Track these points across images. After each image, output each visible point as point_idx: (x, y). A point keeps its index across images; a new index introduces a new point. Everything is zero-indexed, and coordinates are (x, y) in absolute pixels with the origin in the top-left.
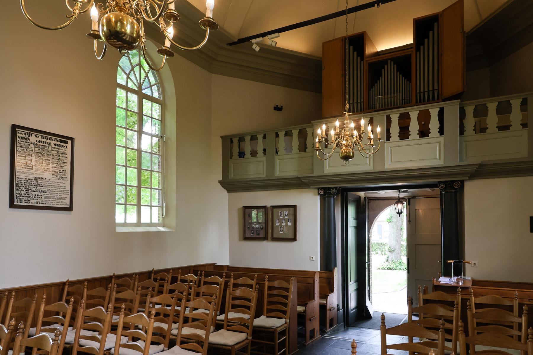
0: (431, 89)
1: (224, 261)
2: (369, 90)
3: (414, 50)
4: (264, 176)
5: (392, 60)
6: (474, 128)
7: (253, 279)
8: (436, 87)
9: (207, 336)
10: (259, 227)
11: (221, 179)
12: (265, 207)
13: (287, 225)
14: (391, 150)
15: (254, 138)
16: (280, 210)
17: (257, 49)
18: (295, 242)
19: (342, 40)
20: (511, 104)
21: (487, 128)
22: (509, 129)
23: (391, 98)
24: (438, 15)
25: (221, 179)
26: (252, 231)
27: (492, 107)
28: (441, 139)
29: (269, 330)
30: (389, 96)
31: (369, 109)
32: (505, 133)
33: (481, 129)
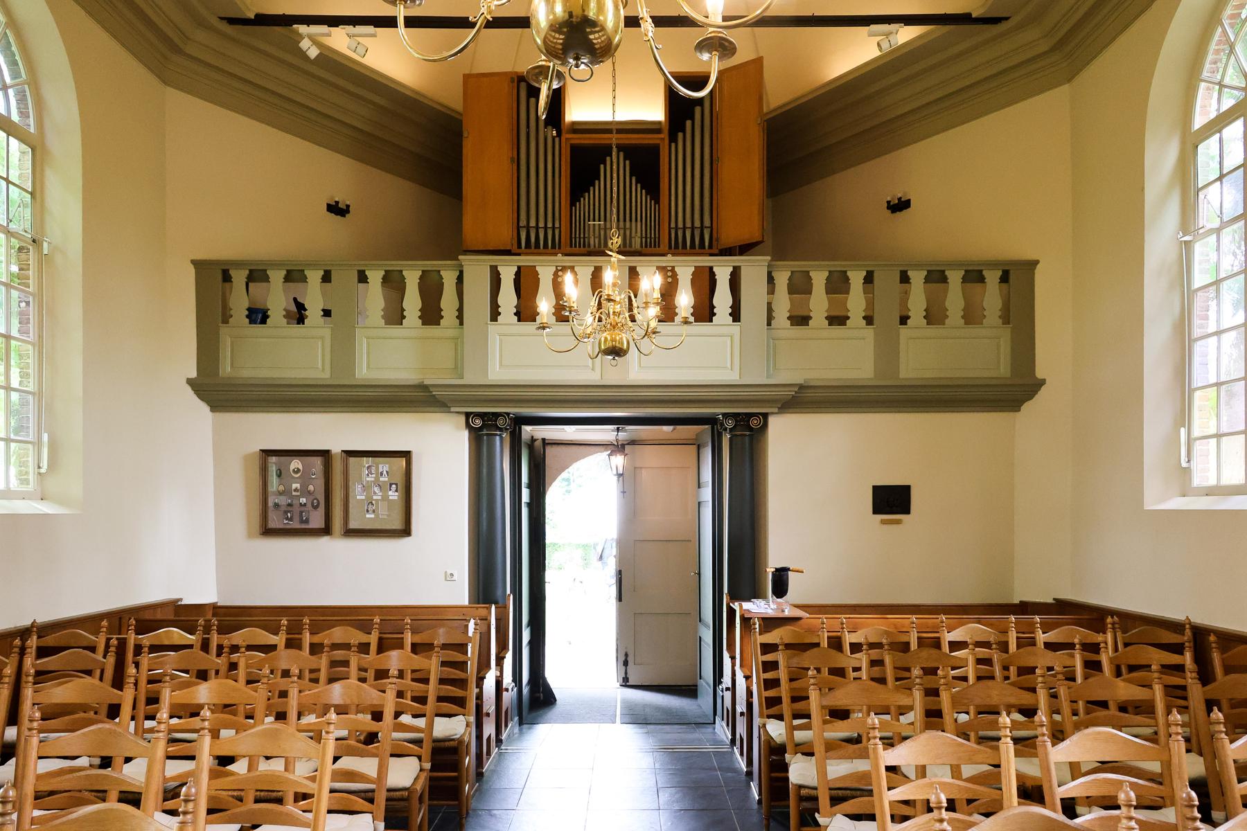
0: (697, 224)
1: (202, 589)
4: (327, 375)
7: (276, 634)
9: (382, 770)
10: (302, 501)
11: (193, 374)
12: (325, 454)
13: (385, 498)
15: (294, 276)
16: (366, 461)
17: (313, 53)
18: (406, 540)
19: (512, 81)
20: (847, 279)
21: (848, 318)
25: (193, 374)
26: (286, 512)
27: (819, 279)
28: (736, 329)
29: (442, 744)
32: (837, 331)
33: (799, 320)
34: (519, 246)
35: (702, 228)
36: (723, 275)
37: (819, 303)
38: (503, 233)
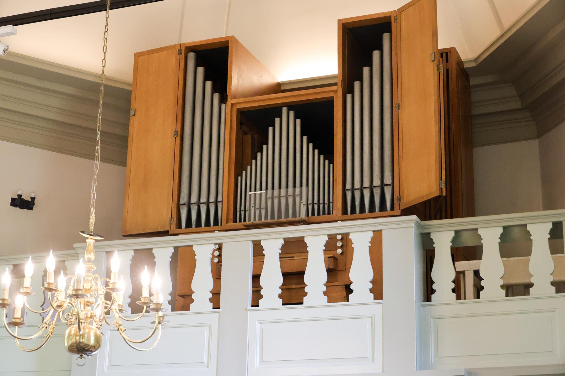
0: (377, 182)
2: (238, 174)
3: (339, 89)
5: (290, 106)
6: (453, 286)
8: (388, 180)
14: (262, 331)
19: (180, 52)
20: (529, 234)
21: (531, 285)
22: (188, 309)
23: (279, 197)
24: (390, 17)
28: (377, 308)
30: (283, 192)
31: (235, 221)
32: (518, 302)
34: (179, 226)
35: (383, 185)
36: (203, 251)
37: (492, 266)
38: (163, 215)
